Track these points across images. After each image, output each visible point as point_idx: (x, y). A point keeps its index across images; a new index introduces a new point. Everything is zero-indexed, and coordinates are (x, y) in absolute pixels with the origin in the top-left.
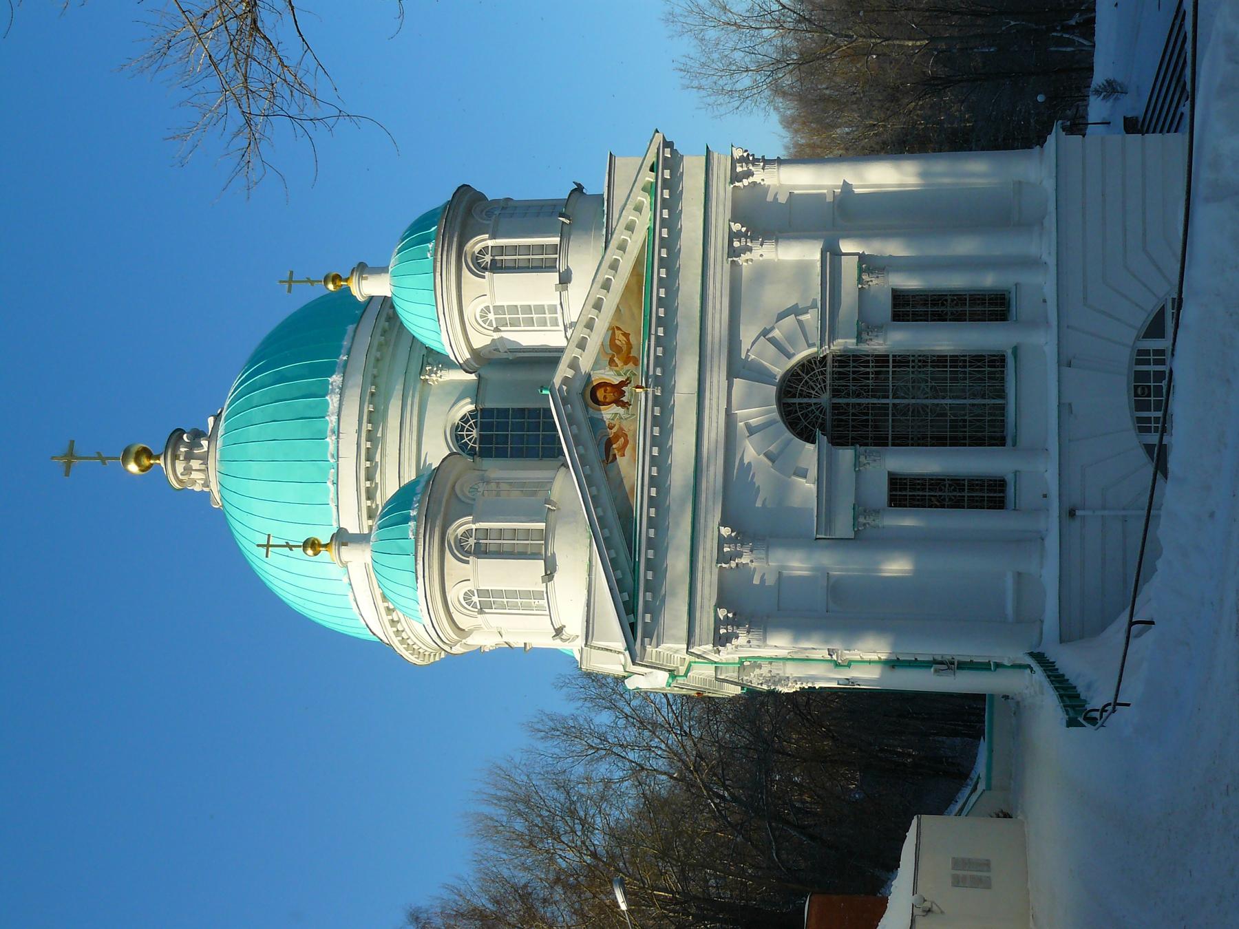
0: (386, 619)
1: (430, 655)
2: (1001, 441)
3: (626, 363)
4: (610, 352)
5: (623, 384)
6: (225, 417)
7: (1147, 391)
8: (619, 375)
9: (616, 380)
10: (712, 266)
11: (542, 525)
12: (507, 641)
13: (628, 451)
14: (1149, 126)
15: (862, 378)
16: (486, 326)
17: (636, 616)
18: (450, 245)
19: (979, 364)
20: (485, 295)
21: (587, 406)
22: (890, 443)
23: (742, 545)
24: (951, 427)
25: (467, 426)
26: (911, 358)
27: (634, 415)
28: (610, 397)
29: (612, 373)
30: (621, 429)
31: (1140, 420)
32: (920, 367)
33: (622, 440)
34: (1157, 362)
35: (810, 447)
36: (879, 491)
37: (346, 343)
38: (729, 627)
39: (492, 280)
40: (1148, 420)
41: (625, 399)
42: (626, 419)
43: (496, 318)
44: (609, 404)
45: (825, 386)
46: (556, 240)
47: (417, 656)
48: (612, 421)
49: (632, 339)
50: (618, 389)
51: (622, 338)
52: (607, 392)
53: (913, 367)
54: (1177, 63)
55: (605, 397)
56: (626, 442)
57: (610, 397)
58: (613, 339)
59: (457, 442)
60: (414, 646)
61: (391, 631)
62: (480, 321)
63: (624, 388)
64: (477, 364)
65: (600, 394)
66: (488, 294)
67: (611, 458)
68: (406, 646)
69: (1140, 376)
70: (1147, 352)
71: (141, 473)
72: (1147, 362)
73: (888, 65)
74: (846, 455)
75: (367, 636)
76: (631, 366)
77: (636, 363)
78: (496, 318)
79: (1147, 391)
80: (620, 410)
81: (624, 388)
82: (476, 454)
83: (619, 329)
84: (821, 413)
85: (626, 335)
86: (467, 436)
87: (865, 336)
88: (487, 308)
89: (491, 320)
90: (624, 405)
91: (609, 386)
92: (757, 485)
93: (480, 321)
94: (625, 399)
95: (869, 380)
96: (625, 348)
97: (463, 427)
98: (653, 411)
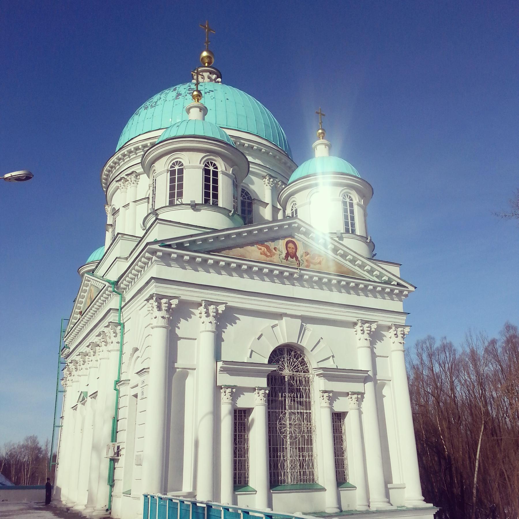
5: (297, 258)
8: (302, 256)
9: (298, 254)
10: (383, 315)
11: (211, 204)
13: (263, 257)
15: (301, 393)
18: (356, 182)
19: (311, 465)
22: (269, 410)
23: (214, 316)
24: (302, 448)
26: (309, 423)
27: (282, 262)
28: (290, 250)
29: (302, 253)
30: (274, 254)
32: (307, 428)
33: (269, 254)
35: (266, 361)
36: (242, 403)
38: (215, 310)
39: (198, 168)
41: (289, 258)
42: (279, 257)
43: (176, 169)
44: (287, 249)
45: (294, 372)
46: (358, 232)
48: (278, 250)
50: (294, 256)
52: (293, 249)
53: (307, 424)
55: (290, 248)
63: (294, 258)
65: (291, 245)
74: (263, 382)
80: (284, 255)
81: (294, 258)
84: (293, 370)
87: (326, 395)
89: (174, 167)
91: (295, 250)
92: (178, 324)
94: (289, 258)
95: (300, 398)
98: (287, 271)
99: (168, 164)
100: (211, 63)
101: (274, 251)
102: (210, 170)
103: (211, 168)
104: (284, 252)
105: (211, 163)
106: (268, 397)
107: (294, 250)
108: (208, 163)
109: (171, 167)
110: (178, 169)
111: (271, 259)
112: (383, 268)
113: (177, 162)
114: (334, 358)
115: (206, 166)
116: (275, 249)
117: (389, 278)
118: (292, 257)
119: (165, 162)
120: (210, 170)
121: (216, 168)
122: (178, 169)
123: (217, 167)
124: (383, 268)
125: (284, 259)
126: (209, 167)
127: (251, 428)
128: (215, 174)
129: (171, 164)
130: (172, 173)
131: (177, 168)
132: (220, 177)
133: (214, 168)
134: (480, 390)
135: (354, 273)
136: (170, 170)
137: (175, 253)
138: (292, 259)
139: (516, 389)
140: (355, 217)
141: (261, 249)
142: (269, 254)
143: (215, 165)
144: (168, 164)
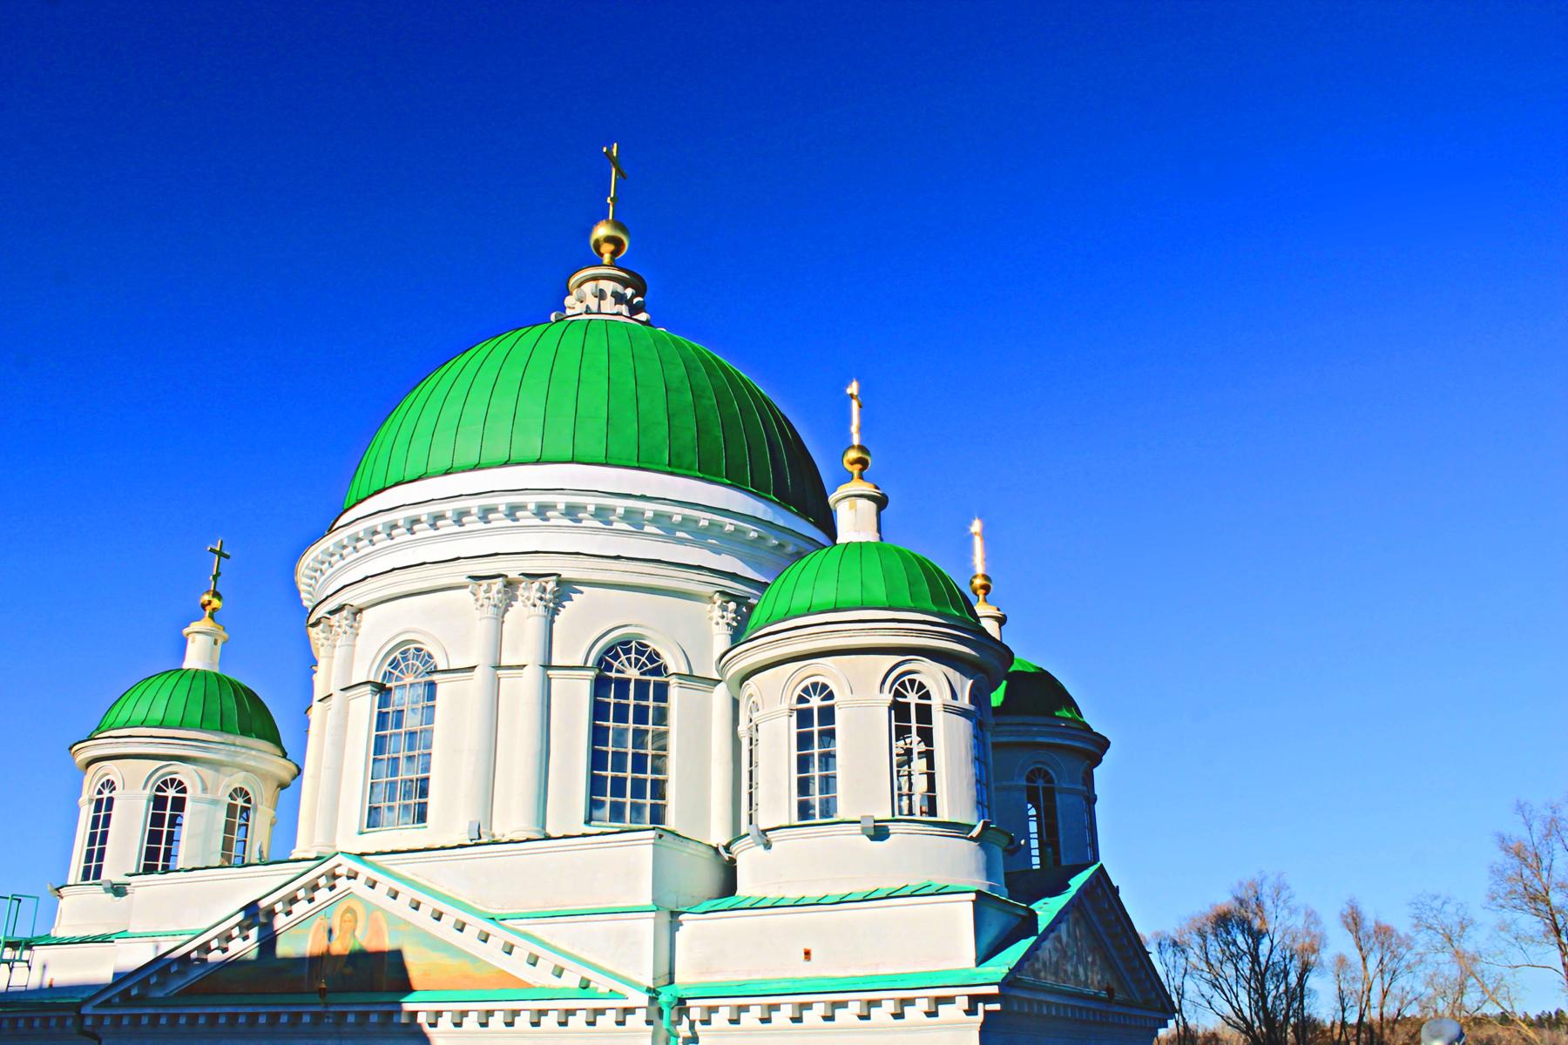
1: (310, 585)
6: (683, 346)
12: (333, 697)
20: (852, 693)
25: (643, 659)
37: (783, 503)
43: (167, 797)
47: (311, 565)
59: (604, 653)
60: (327, 564)
64: (730, 678)
66: (855, 697)
68: (331, 549)
71: (592, 242)
75: (360, 485)
78: (167, 797)
82: (600, 670)
86: (629, 660)
88: (184, 790)
89: (165, 791)
97: (642, 654)
99: (92, 788)
100: (623, 249)
102: (909, 703)
103: (912, 698)
105: (912, 682)
108: (903, 685)
109: (801, 700)
110: (173, 798)
112: (289, 874)
113: (815, 685)
115: (898, 694)
119: (144, 781)
120: (909, 703)
121: (927, 696)
122: (173, 798)
123: (928, 691)
124: (289, 874)
126: (905, 697)
127: (104, 985)
128: (925, 713)
129: (798, 691)
130: (804, 717)
132: (939, 720)
133: (920, 698)
136: (797, 710)
140: (936, 776)
143: (922, 686)
144: (793, 687)
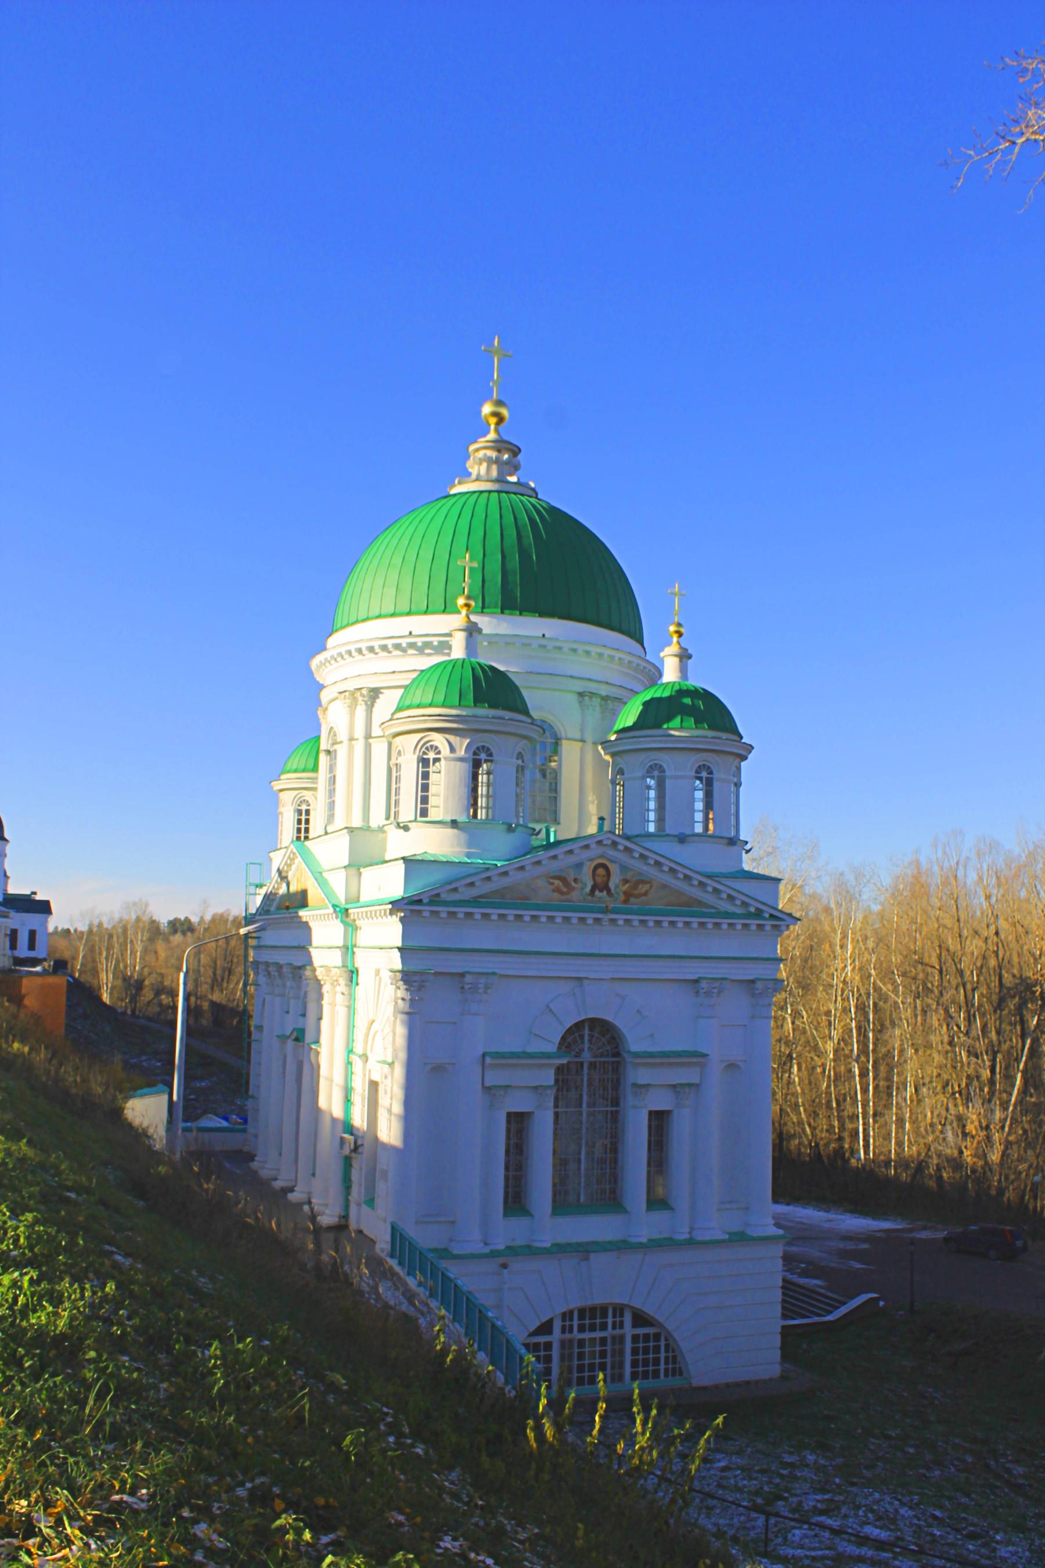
0: (343, 650)
2: (554, 1208)
3: (625, 893)
4: (634, 879)
7: (593, 1317)
8: (617, 887)
9: (612, 885)
14: (791, 1290)
16: (423, 749)
17: (428, 904)
21: (592, 860)
28: (599, 880)
29: (617, 881)
31: (571, 1312)
33: (565, 890)
34: (614, 1323)
40: (571, 1319)
41: (597, 893)
49: (643, 898)
50: (606, 887)
51: (644, 890)
54: (820, 1308)
55: (599, 875)
56: (562, 893)
57: (599, 880)
58: (644, 882)
61: (335, 652)
62: (428, 745)
63: (605, 892)
65: (601, 871)
67: (551, 881)
69: (604, 1310)
70: (622, 1315)
72: (614, 1316)
73: (942, 1096)
76: (622, 897)
77: (626, 902)
79: (593, 1317)
80: (588, 889)
83: (651, 887)
85: (646, 894)
88: (439, 753)
90: (592, 891)
93: (428, 745)
94: (597, 893)
96: (636, 892)
101: (573, 884)
103: (304, 807)
104: (590, 884)
106: (618, 1062)
107: (605, 879)
109: (299, 805)
111: (568, 897)
114: (726, 841)
116: (576, 880)
117: (757, 909)
118: (601, 891)
125: (589, 895)
131: (304, 807)
134: (1009, 1120)
135: (700, 903)
137: (426, 910)
138: (601, 894)
139: (1011, 1040)
141: (552, 884)
142: (565, 890)
